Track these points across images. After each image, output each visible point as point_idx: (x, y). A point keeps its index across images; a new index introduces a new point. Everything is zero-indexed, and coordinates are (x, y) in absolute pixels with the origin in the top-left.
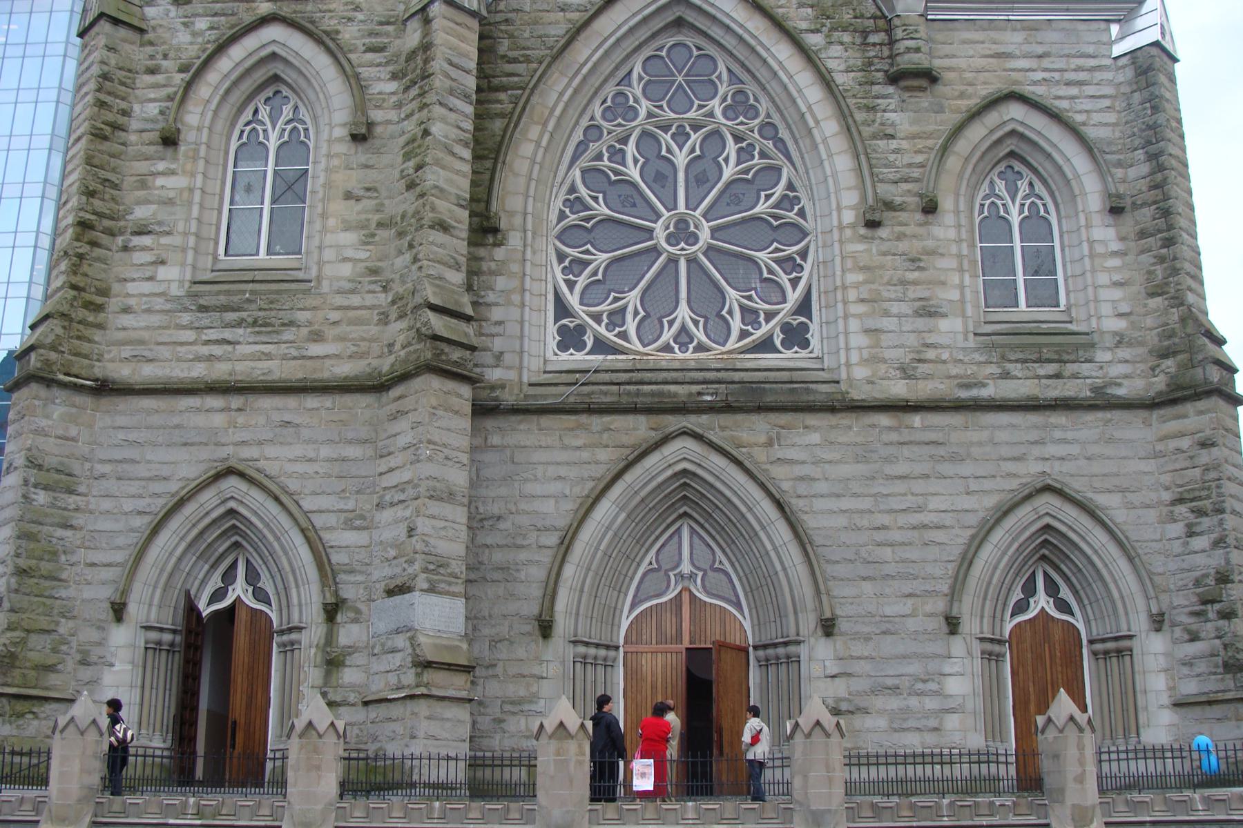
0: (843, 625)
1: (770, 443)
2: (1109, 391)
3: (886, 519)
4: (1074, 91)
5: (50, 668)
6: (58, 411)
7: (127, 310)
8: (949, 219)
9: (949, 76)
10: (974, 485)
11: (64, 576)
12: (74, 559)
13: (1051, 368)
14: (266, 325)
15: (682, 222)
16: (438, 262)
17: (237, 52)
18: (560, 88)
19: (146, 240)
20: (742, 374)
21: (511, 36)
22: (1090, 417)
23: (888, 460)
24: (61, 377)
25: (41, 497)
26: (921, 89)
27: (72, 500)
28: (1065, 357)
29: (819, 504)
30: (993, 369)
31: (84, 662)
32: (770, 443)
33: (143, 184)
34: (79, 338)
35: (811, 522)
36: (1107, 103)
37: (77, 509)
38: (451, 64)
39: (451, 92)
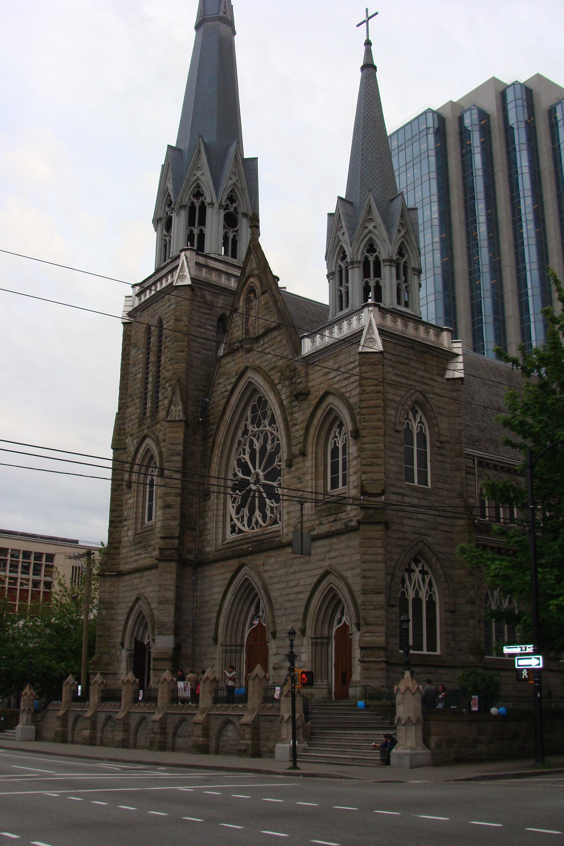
0: (278, 635)
1: (264, 564)
2: (349, 524)
3: (288, 591)
4: (346, 382)
5: (110, 664)
6: (107, 585)
7: (123, 547)
8: (310, 457)
9: (312, 390)
10: (311, 573)
11: (112, 635)
12: (115, 629)
13: (333, 517)
14: (146, 547)
15: (258, 475)
16: (168, 520)
17: (141, 450)
18: (222, 432)
19: (126, 523)
20: (267, 535)
21: (213, 414)
22: (343, 538)
23: (291, 566)
24: (107, 573)
25: (104, 612)
26: (305, 399)
27: (113, 611)
28: (338, 511)
29: (275, 587)
30: (317, 522)
31: (118, 662)
32: (264, 564)
33: (126, 504)
34: (112, 559)
35: (273, 594)
36: (356, 384)
37: (114, 614)
38: (171, 444)
39: (172, 455)
